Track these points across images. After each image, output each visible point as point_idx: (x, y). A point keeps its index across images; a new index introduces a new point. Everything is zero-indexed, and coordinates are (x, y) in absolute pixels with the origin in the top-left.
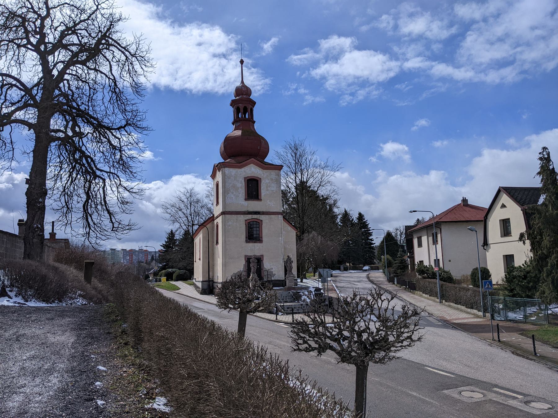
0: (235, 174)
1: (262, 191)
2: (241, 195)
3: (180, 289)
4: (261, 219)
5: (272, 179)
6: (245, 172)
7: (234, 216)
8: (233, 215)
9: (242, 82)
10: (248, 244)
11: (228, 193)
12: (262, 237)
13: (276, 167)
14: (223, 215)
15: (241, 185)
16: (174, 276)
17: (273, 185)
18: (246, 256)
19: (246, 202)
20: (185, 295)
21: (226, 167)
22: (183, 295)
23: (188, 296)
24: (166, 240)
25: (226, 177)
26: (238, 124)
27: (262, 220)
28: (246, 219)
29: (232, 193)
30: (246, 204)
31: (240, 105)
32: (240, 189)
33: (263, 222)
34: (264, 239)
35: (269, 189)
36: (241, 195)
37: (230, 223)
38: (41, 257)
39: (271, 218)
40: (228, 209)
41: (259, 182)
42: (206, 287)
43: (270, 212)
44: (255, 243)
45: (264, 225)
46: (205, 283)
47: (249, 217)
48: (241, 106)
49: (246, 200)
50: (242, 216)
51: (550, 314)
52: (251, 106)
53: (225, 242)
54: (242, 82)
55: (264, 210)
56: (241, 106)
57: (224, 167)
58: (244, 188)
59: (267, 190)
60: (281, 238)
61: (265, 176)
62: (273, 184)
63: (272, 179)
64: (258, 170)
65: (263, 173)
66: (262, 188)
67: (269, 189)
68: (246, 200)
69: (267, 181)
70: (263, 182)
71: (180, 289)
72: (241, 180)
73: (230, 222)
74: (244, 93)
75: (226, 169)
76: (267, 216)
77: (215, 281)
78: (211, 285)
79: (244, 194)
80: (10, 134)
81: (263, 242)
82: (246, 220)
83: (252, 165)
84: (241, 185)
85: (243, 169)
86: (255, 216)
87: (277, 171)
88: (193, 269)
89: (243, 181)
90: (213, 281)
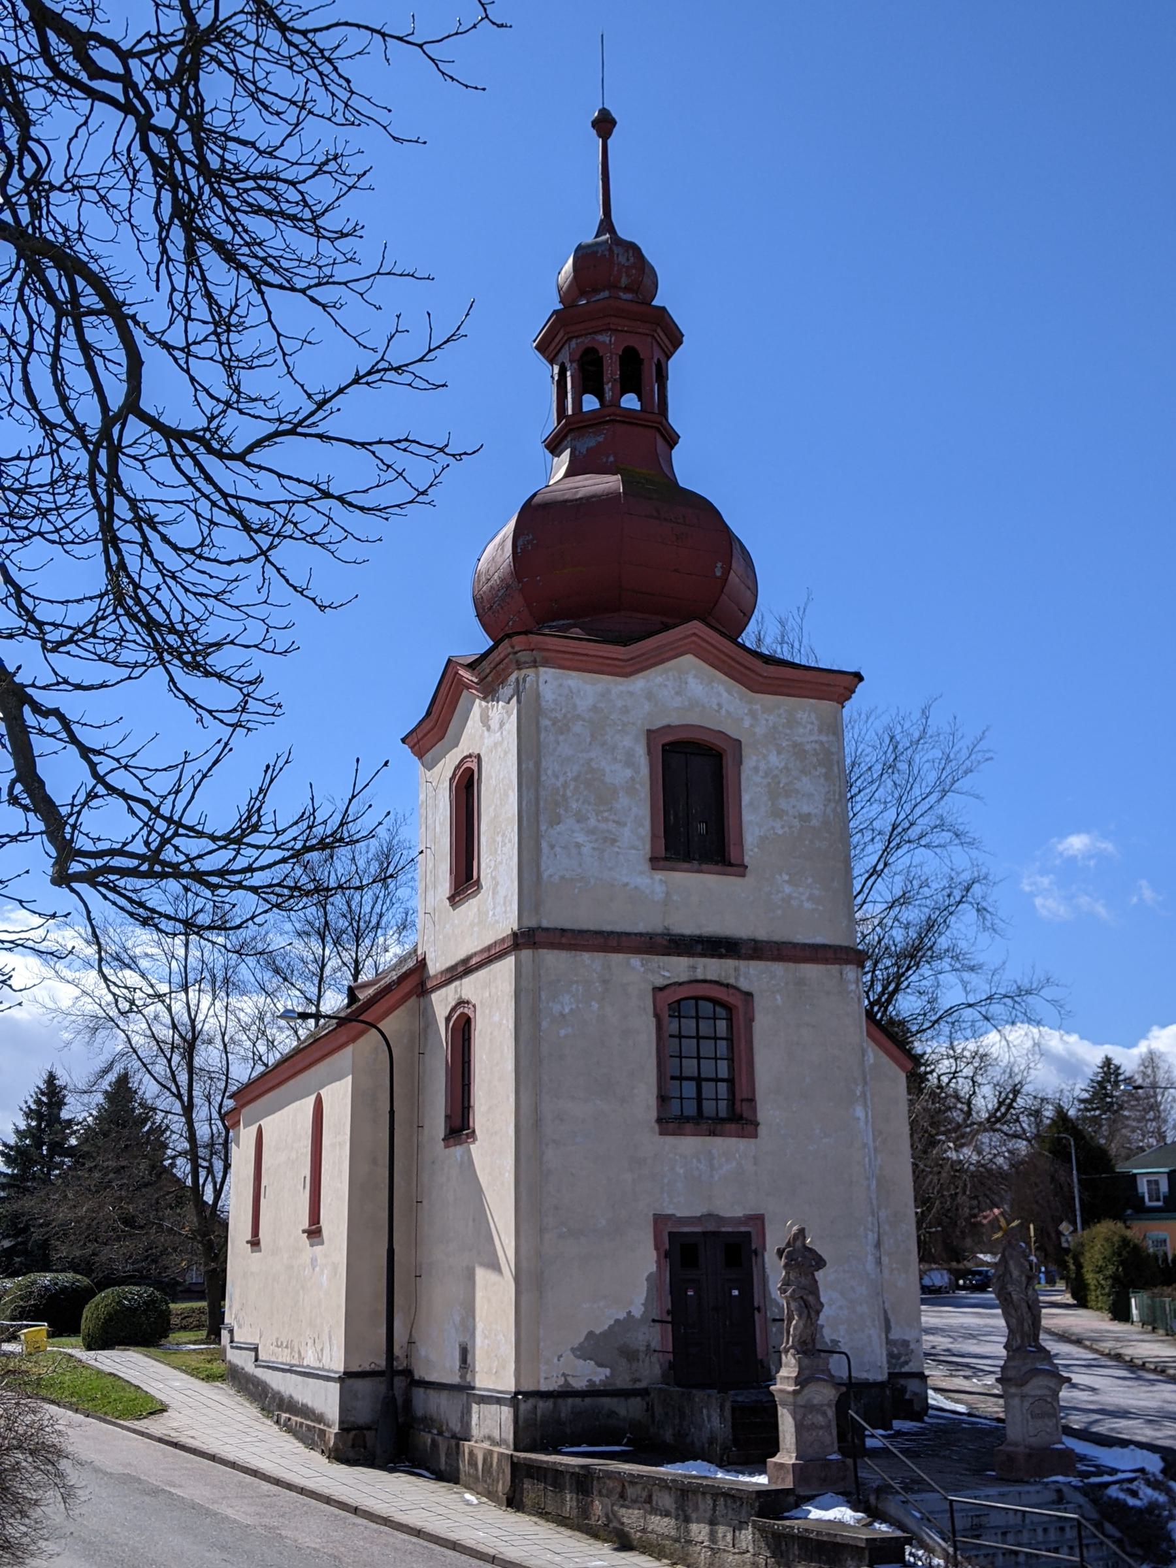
0: (594, 709)
1: (747, 816)
2: (626, 832)
3: (163, 1409)
4: (744, 985)
5: (799, 751)
6: (650, 696)
7: (591, 962)
8: (586, 956)
9: (607, 225)
10: (670, 1140)
11: (556, 821)
12: (752, 1100)
13: (809, 675)
14: (526, 954)
15: (629, 773)
16: (90, 1314)
17: (805, 784)
18: (660, 1220)
19: (659, 876)
20: (233, 1465)
21: (546, 663)
22: (213, 1458)
23: (255, 1473)
24: (43, 1086)
25: (545, 722)
26: (590, 442)
27: (749, 995)
28: (660, 982)
29: (581, 818)
30: (659, 891)
31: (604, 338)
32: (623, 801)
33: (760, 1003)
34: (767, 1111)
35: (783, 804)
36: (626, 832)
37: (566, 1004)
38: (215, 1324)
39: (801, 982)
40: (554, 917)
41: (728, 761)
42: (364, 1413)
43: (795, 945)
44: (712, 1133)
45: (762, 1023)
46: (361, 1385)
47: (678, 968)
48: (608, 343)
49: (656, 862)
50: (635, 961)
51: (192, 1293)
52: (658, 354)
53: (537, 1123)
54: (607, 225)
55: (762, 934)
56: (608, 343)
57: (535, 664)
58: (644, 791)
59: (777, 813)
60: (859, 1112)
61: (760, 731)
62: (805, 779)
63: (799, 751)
64: (721, 688)
65: (753, 714)
66: (746, 799)
67: (783, 804)
68: (656, 862)
69: (774, 759)
70: (750, 761)
71: (163, 1409)
72: (627, 742)
73: (566, 998)
74: (624, 281)
75: (546, 673)
76: (778, 968)
77: (420, 1373)
78: (400, 1402)
79: (645, 830)
80: (155, 212)
81: (762, 1130)
82: (658, 990)
83: (689, 658)
84: (629, 773)
85: (638, 683)
86: (711, 968)
87: (827, 705)
88: (224, 1270)
89: (641, 751)
90: (408, 1373)
